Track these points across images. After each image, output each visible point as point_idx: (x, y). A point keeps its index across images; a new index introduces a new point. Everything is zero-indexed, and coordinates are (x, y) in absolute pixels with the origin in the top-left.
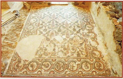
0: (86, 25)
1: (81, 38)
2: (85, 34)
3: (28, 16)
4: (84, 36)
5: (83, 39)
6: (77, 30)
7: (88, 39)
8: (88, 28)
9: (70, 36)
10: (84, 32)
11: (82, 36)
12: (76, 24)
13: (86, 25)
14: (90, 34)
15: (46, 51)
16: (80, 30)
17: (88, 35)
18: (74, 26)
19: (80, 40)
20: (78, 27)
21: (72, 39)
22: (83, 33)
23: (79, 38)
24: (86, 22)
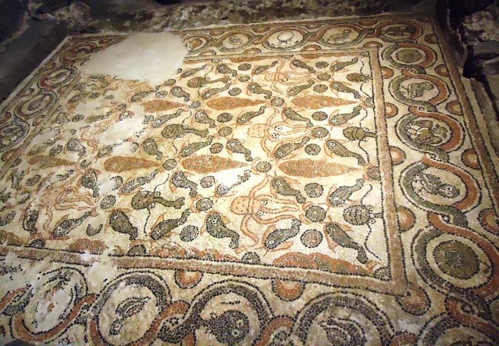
0: (159, 291)
1: (67, 224)
2: (86, 257)
3: (230, 53)
4: (75, 249)
5: (54, 235)
6: (139, 219)
7: (39, 265)
8: (123, 293)
9: (114, 175)
10: (104, 257)
11: (78, 233)
12: (197, 220)
13: (159, 291)
14: (63, 298)
15: (380, 182)
16: (132, 232)
17: (65, 280)
18: (178, 203)
19: (58, 216)
20: (164, 229)
21: (88, 181)
22: (97, 248)
23: (74, 214)
24: (202, 304)
